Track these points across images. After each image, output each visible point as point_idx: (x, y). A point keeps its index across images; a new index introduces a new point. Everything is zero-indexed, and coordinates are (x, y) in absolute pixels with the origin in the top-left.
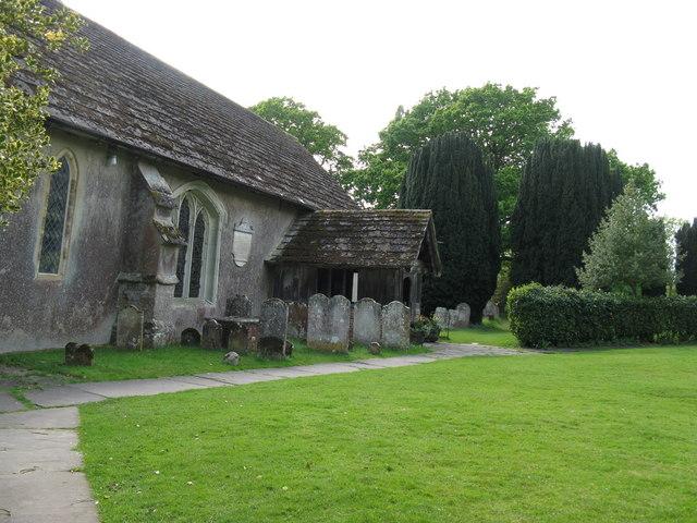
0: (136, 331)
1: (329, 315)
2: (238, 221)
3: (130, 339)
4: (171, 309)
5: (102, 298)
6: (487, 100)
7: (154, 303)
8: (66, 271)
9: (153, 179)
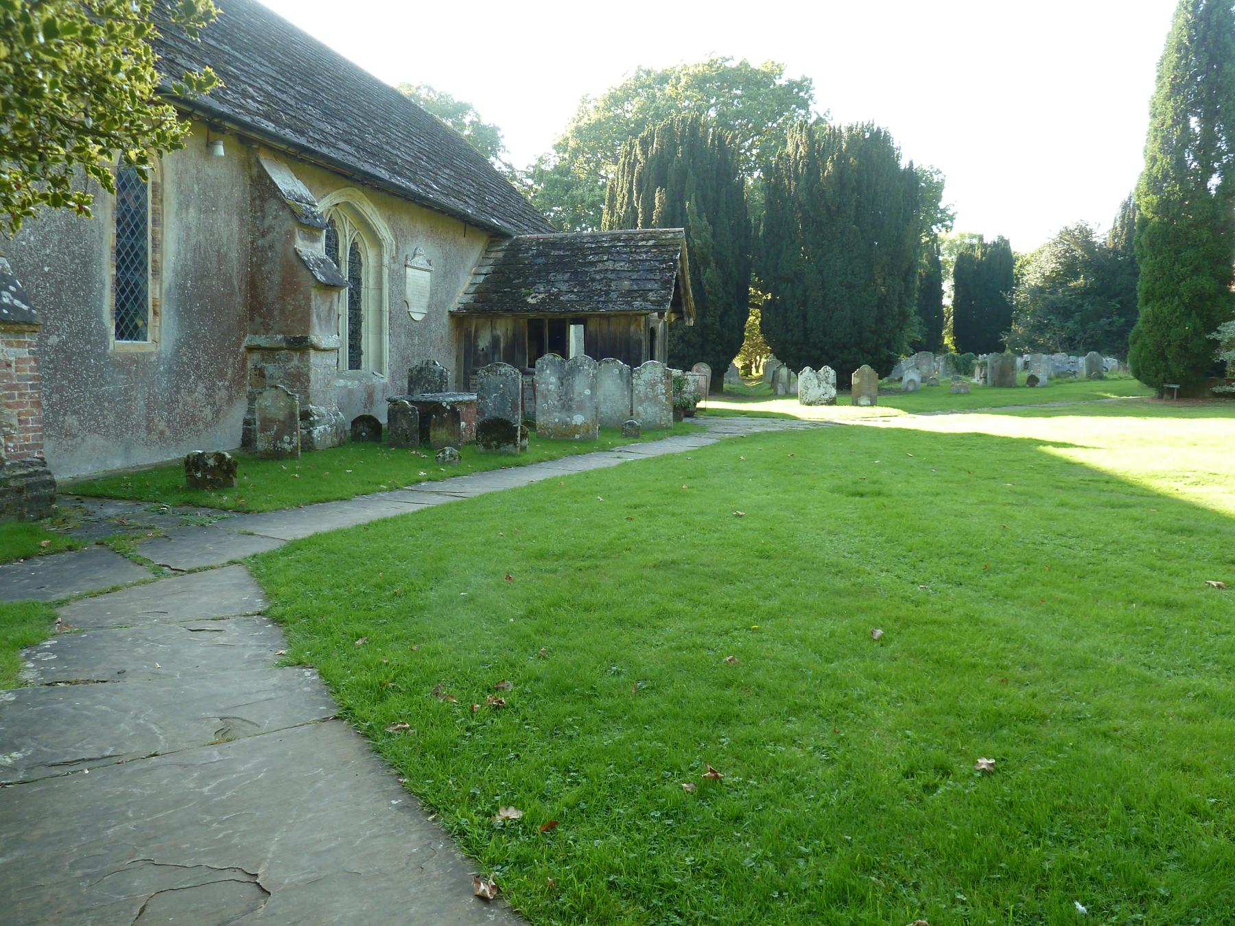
0: (288, 425)
2: (410, 253)
3: (278, 436)
4: (333, 385)
5: (222, 375)
7: (308, 381)
8: (162, 334)
9: (286, 181)
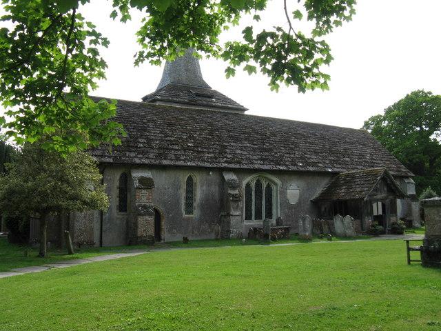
1: (343, 223)
6: (416, 94)
8: (196, 214)
